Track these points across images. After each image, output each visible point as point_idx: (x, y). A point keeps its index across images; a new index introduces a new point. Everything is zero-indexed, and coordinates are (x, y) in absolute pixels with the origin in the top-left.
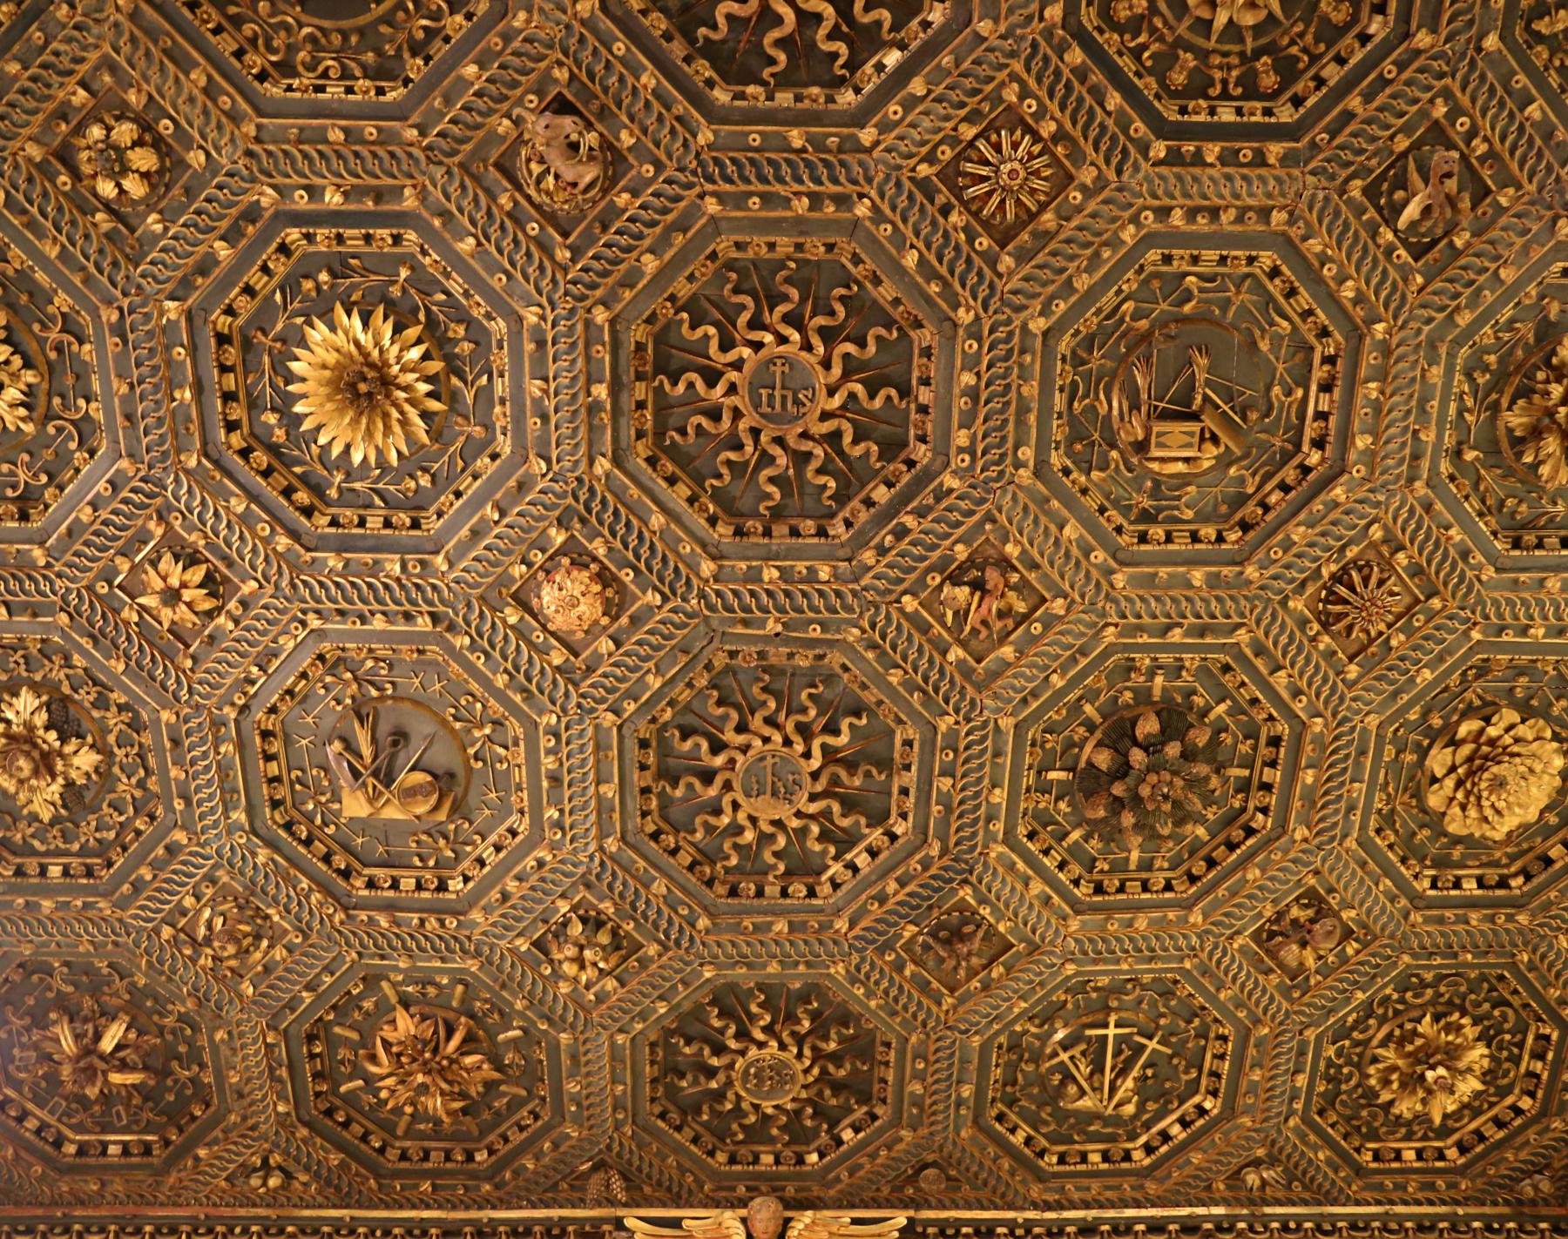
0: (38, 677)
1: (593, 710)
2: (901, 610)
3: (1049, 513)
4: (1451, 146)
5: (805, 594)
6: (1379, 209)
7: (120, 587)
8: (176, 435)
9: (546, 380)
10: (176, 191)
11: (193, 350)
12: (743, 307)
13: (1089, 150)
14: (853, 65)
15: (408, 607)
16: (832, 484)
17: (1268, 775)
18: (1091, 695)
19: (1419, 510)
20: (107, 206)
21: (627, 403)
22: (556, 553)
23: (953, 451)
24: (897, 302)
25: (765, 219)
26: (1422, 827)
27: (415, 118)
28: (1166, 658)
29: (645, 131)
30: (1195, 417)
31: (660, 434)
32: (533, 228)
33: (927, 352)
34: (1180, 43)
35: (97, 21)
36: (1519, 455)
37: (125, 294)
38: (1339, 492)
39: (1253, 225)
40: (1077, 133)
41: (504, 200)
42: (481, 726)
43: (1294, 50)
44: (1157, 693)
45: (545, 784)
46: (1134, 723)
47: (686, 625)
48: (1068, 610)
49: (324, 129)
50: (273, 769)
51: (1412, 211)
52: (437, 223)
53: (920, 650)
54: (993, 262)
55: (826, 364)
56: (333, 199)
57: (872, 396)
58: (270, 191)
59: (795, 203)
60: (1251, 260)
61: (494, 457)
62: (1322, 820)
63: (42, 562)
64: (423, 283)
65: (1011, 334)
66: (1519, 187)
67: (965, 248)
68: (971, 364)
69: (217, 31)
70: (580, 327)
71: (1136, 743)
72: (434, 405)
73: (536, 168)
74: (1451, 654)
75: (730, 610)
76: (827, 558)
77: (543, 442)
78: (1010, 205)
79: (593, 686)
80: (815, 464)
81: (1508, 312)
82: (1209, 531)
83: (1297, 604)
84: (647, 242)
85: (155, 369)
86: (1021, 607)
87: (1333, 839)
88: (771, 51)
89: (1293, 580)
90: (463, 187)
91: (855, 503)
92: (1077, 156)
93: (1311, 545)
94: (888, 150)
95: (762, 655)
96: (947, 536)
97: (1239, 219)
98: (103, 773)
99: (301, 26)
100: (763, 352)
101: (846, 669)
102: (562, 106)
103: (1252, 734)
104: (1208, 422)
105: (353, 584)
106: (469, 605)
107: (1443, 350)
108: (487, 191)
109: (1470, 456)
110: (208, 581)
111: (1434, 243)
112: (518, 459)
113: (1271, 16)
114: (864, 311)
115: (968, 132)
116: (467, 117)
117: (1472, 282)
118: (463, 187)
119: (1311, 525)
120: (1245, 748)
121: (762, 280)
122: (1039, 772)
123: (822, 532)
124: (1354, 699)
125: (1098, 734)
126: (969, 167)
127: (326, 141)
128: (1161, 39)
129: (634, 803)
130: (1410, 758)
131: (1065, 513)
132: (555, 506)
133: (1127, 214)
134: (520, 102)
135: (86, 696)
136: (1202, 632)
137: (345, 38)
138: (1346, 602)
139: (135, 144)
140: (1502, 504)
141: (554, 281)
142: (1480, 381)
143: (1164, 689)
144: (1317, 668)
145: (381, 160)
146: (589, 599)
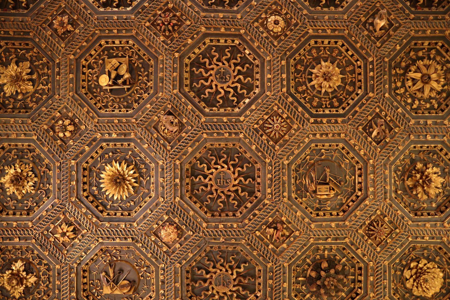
0: (24, 257)
1: (174, 263)
2: (256, 235)
3: (293, 209)
4: (381, 118)
5: (230, 231)
6: (367, 133)
7: (50, 232)
8: (70, 193)
9: (164, 178)
10: (77, 135)
11: (77, 172)
12: (213, 159)
13: (295, 120)
14: (238, 102)
15: (126, 236)
16: (236, 203)
17: (360, 278)
18: (308, 257)
19: (389, 206)
20: (61, 139)
21: (184, 183)
22: (165, 222)
23: (267, 194)
24: (251, 157)
25: (218, 139)
26: (406, 293)
27: (135, 117)
28: (327, 246)
29: (189, 119)
30: (327, 184)
31: (192, 191)
32: (162, 142)
33: (259, 170)
34: (314, 96)
36: (412, 192)
37: (62, 159)
38: (367, 202)
39: (337, 137)
40: (292, 117)
41: (155, 135)
42: (143, 268)
43: (341, 97)
44: (326, 256)
45: (160, 283)
46: (321, 264)
47: (199, 240)
48: (300, 234)
49: (114, 120)
50: (85, 280)
51: (375, 133)
52: (139, 141)
53: (261, 246)
54: (274, 148)
55: (234, 173)
56: (114, 136)
57: (246, 181)
59: (225, 134)
60: (337, 145)
61: (150, 197)
62: (377, 291)
63: (31, 226)
64: (135, 155)
65: (279, 165)
66: (399, 127)
67: (267, 144)
68: (270, 172)
69: (91, 99)
70: (173, 165)
71: (322, 270)
72: (136, 185)
73: (163, 128)
74: (404, 244)
75: (210, 236)
76: (236, 222)
77: (163, 194)
78: (277, 134)
79: (174, 256)
80: (232, 198)
81: (402, 157)
82: (335, 213)
83: (360, 231)
84: (189, 145)
85: (67, 177)
86: (287, 234)
87: (381, 297)
88: (219, 100)
89: (358, 225)
90: (145, 132)
91: (242, 207)
92: (292, 122)
93: (362, 216)
94: (247, 122)
95: (219, 247)
96: (267, 216)
97: (333, 136)
98: (37, 284)
99: (110, 97)
100: (218, 170)
101: (242, 251)
102: (169, 113)
103: (353, 266)
104: (331, 185)
105: (112, 230)
106: (142, 235)
107: (388, 166)
108: (151, 133)
109: (399, 192)
110: (74, 231)
111: (381, 141)
112: (156, 198)
113: (335, 90)
114: (243, 160)
115: (266, 117)
116: (147, 116)
117: (392, 150)
118: (145, 132)
119: (361, 210)
120: (352, 270)
121: (217, 153)
122: (296, 278)
123: (234, 215)
124: (380, 257)
125: (311, 267)
126: (267, 125)
127: (114, 123)
128: (310, 95)
129: (185, 289)
130: (399, 273)
131: (297, 209)
132: (165, 210)
133: (306, 135)
134: (160, 113)
135: (36, 262)
136: (336, 239)
137: (120, 99)
138: (373, 231)
139: (69, 125)
140: (410, 204)
141: (166, 154)
142: (399, 173)
143: (328, 255)
144: (369, 248)
146: (174, 233)
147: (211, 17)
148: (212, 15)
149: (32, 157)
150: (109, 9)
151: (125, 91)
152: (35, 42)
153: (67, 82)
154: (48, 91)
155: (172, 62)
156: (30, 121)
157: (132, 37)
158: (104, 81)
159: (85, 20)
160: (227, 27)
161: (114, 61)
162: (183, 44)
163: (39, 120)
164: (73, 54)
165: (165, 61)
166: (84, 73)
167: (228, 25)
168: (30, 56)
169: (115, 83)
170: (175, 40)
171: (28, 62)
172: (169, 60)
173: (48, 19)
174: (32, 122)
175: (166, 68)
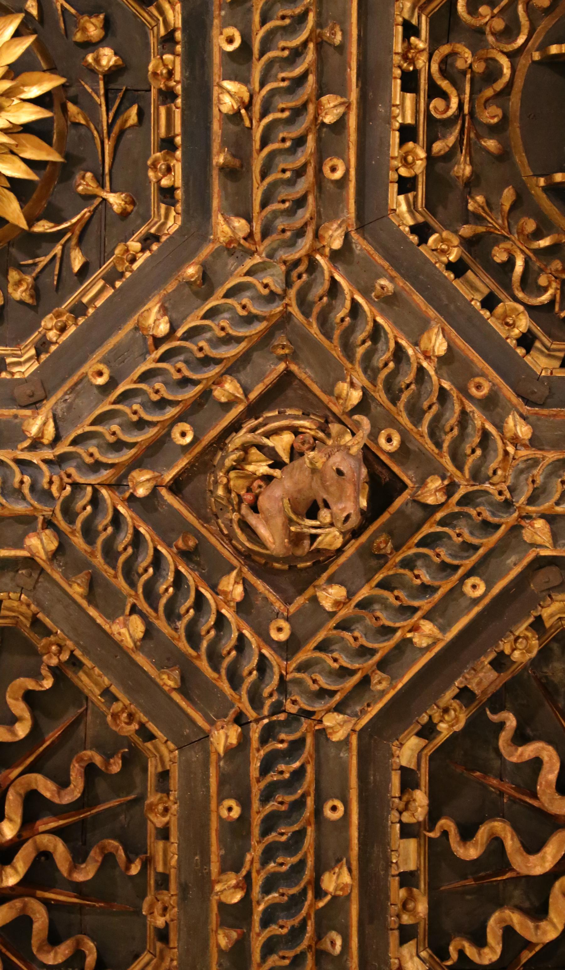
27: (360, 244)
49: (342, 91)
56: (228, 95)
88: (483, 834)
102: (382, 488)
108: (244, 360)
118: (250, 319)
141: (97, 466)
145: (291, 183)
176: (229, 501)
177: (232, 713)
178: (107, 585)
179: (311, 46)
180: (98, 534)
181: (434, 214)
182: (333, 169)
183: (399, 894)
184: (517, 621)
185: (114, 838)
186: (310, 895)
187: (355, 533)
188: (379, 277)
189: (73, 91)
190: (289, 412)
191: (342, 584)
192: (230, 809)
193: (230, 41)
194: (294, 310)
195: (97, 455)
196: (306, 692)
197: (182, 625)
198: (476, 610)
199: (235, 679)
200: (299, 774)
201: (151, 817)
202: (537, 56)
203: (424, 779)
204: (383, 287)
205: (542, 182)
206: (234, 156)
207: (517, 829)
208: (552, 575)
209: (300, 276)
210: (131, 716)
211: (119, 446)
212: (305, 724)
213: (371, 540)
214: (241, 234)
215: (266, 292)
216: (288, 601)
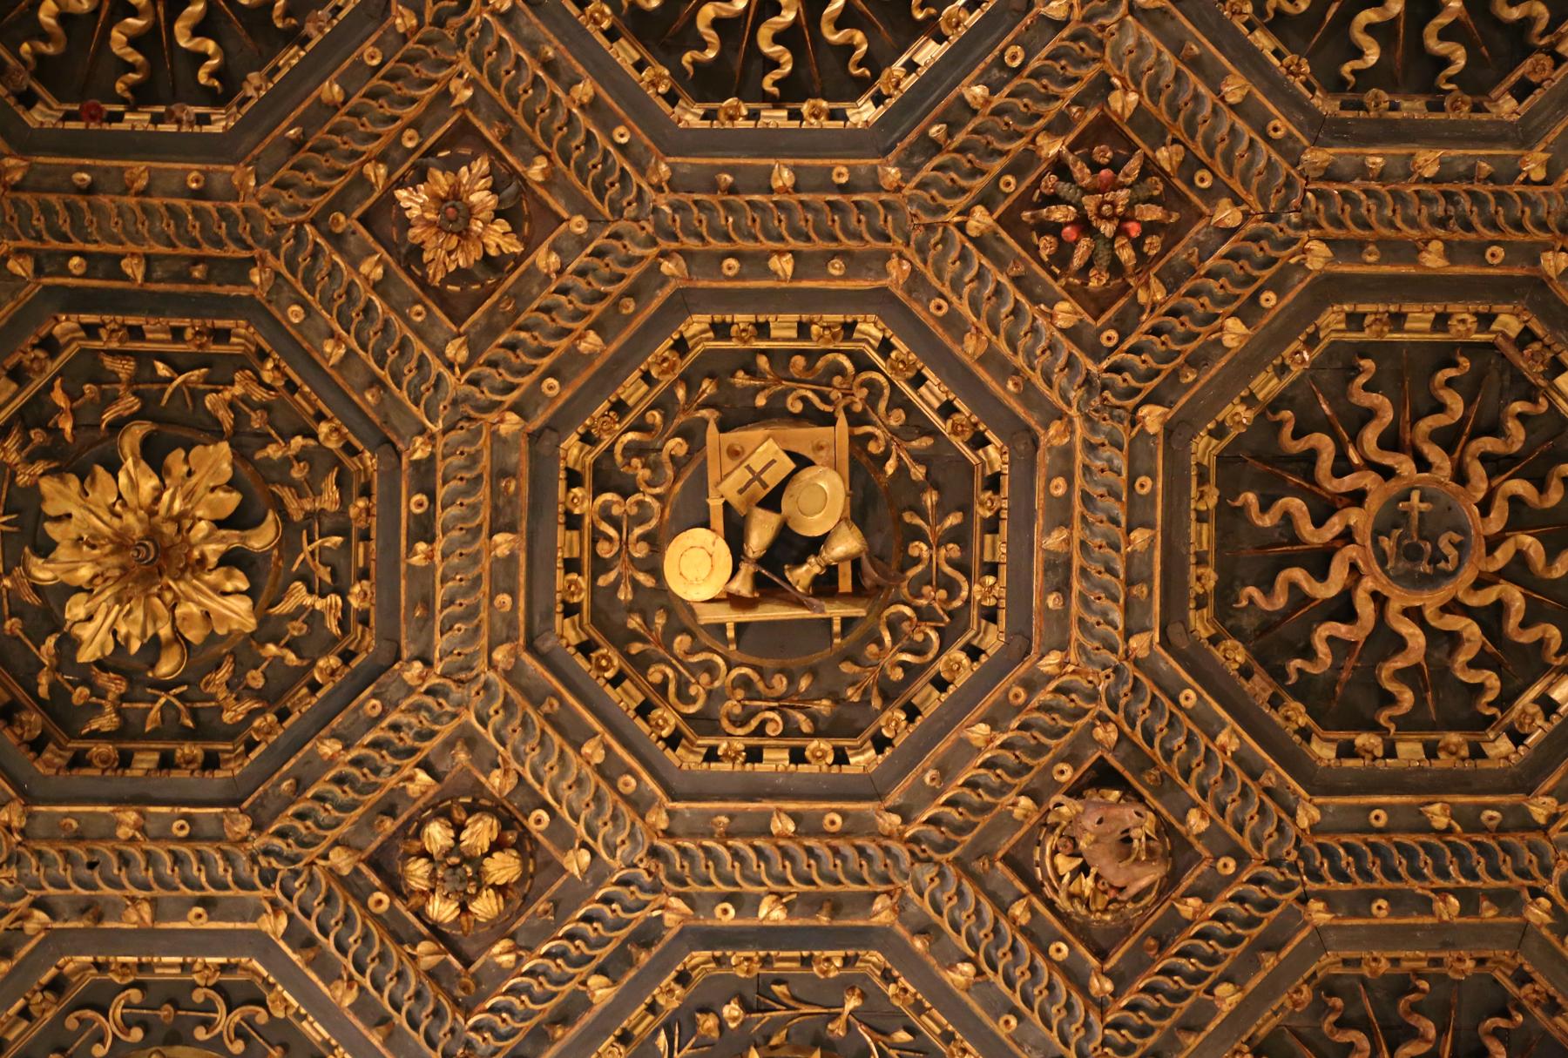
10: (541, 906)
14: (875, 62)
20: (436, 931)
27: (895, 797)
29: (1222, 810)
35: (460, 682)
49: (768, 816)
56: (771, 913)
58: (675, 902)
69: (615, 682)
88: (1392, 687)
102: (1103, 776)
108: (993, 897)
118: (960, 893)
141: (1087, 1025)
145: (844, 859)
147: (1363, 172)
148: (1376, 161)
149: (240, 1033)
150: (736, 114)
151: (821, 638)
152: (276, 328)
153: (477, 581)
154: (343, 624)
155: (1121, 462)
156: (243, 826)
157: (881, 301)
158: (698, 568)
159: (600, 192)
160: (1459, 235)
161: (766, 451)
162: (1191, 347)
163: (301, 816)
164: (516, 408)
165: (1079, 457)
166: (573, 522)
167: (1468, 227)
168: (231, 405)
169: (768, 586)
170: (1147, 321)
171: (225, 447)
172: (1107, 452)
173: (361, 179)
174: (258, 827)
175: (1087, 498)
176: (1118, 910)
177: (1297, 907)
178: (1185, 1016)
179: (730, 843)
180: (1145, 1024)
181: (862, 730)
182: (833, 823)
183: (1444, 761)
184: (1213, 660)
185: (1397, 1004)
186: (1451, 838)
187: (1141, 799)
188: (923, 782)
189: (759, 1040)
190: (1037, 857)
191: (1186, 813)
192: (1379, 908)
193: (725, 911)
194: (951, 855)
195: (1078, 1025)
196: (1279, 844)
197: (1221, 950)
198: (1206, 696)
199: (1269, 905)
200: (1349, 848)
201: (1381, 972)
202: (733, 647)
203: (1343, 735)
204: (933, 779)
205: (837, 641)
206: (821, 908)
207: (1386, 659)
208: (1175, 631)
209: (924, 851)
210: (1298, 991)
211: (1069, 1006)
212: (1306, 843)
213: (1147, 786)
214: (889, 902)
215: (937, 881)
216: (1198, 858)
